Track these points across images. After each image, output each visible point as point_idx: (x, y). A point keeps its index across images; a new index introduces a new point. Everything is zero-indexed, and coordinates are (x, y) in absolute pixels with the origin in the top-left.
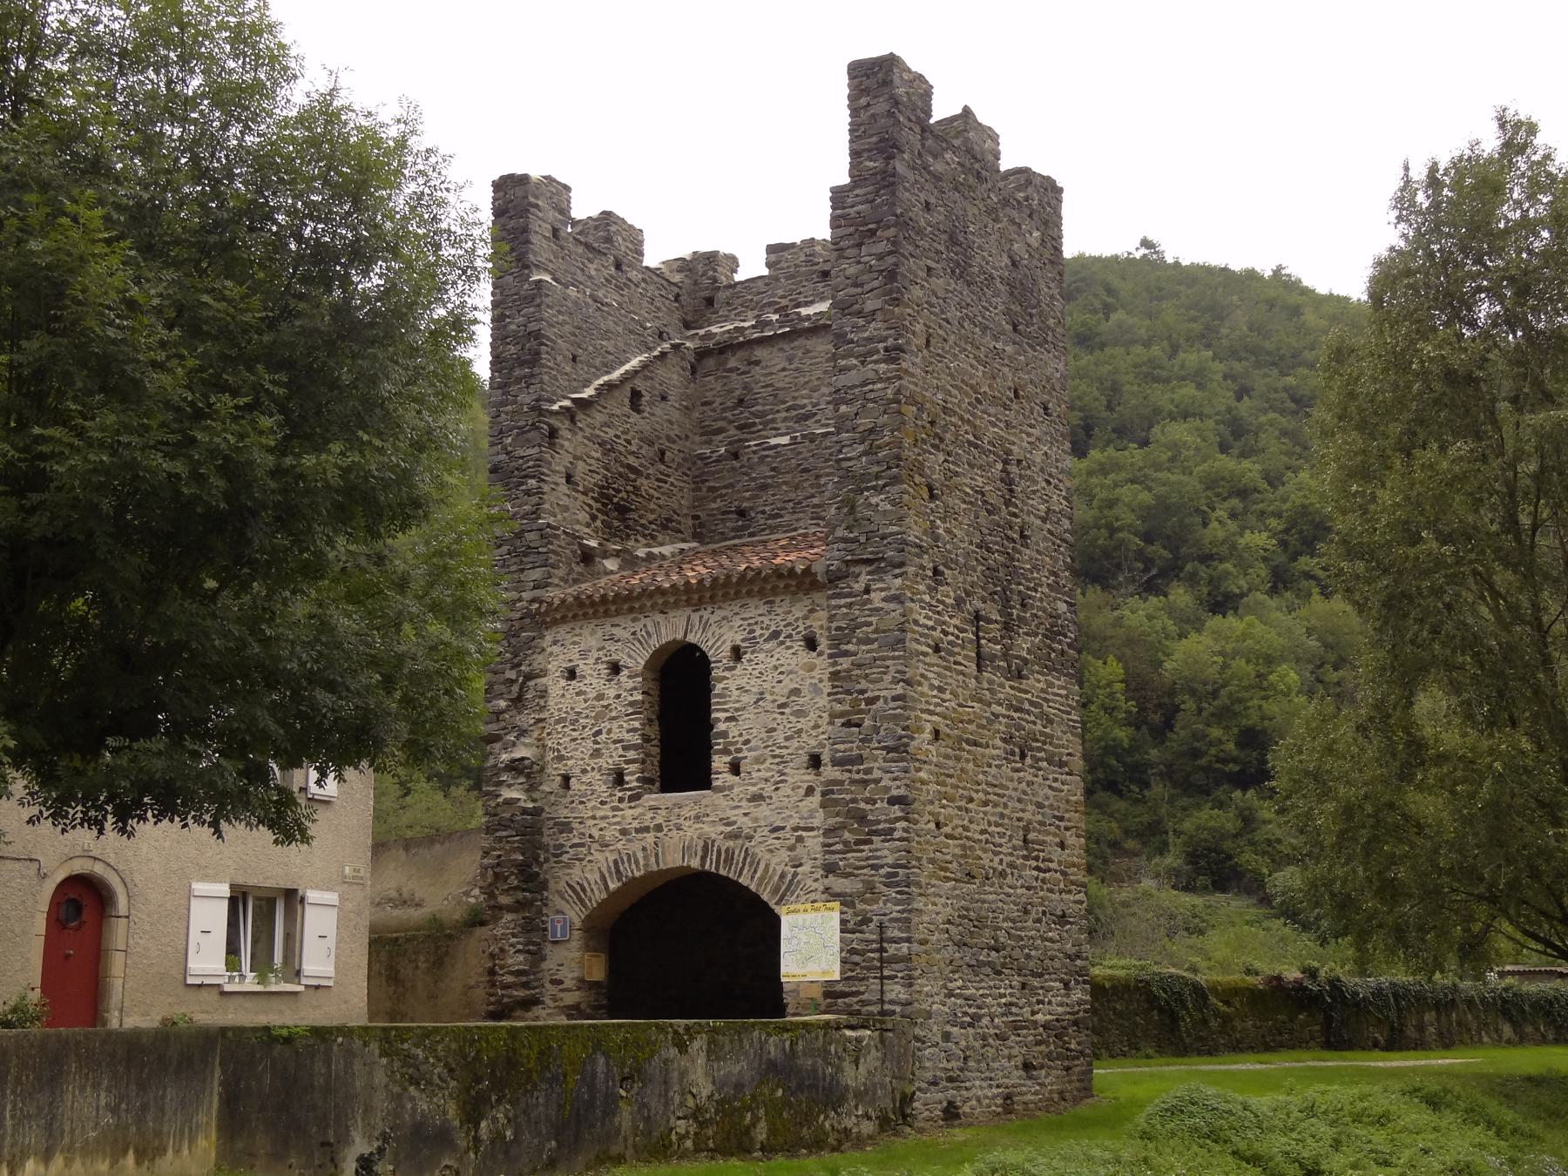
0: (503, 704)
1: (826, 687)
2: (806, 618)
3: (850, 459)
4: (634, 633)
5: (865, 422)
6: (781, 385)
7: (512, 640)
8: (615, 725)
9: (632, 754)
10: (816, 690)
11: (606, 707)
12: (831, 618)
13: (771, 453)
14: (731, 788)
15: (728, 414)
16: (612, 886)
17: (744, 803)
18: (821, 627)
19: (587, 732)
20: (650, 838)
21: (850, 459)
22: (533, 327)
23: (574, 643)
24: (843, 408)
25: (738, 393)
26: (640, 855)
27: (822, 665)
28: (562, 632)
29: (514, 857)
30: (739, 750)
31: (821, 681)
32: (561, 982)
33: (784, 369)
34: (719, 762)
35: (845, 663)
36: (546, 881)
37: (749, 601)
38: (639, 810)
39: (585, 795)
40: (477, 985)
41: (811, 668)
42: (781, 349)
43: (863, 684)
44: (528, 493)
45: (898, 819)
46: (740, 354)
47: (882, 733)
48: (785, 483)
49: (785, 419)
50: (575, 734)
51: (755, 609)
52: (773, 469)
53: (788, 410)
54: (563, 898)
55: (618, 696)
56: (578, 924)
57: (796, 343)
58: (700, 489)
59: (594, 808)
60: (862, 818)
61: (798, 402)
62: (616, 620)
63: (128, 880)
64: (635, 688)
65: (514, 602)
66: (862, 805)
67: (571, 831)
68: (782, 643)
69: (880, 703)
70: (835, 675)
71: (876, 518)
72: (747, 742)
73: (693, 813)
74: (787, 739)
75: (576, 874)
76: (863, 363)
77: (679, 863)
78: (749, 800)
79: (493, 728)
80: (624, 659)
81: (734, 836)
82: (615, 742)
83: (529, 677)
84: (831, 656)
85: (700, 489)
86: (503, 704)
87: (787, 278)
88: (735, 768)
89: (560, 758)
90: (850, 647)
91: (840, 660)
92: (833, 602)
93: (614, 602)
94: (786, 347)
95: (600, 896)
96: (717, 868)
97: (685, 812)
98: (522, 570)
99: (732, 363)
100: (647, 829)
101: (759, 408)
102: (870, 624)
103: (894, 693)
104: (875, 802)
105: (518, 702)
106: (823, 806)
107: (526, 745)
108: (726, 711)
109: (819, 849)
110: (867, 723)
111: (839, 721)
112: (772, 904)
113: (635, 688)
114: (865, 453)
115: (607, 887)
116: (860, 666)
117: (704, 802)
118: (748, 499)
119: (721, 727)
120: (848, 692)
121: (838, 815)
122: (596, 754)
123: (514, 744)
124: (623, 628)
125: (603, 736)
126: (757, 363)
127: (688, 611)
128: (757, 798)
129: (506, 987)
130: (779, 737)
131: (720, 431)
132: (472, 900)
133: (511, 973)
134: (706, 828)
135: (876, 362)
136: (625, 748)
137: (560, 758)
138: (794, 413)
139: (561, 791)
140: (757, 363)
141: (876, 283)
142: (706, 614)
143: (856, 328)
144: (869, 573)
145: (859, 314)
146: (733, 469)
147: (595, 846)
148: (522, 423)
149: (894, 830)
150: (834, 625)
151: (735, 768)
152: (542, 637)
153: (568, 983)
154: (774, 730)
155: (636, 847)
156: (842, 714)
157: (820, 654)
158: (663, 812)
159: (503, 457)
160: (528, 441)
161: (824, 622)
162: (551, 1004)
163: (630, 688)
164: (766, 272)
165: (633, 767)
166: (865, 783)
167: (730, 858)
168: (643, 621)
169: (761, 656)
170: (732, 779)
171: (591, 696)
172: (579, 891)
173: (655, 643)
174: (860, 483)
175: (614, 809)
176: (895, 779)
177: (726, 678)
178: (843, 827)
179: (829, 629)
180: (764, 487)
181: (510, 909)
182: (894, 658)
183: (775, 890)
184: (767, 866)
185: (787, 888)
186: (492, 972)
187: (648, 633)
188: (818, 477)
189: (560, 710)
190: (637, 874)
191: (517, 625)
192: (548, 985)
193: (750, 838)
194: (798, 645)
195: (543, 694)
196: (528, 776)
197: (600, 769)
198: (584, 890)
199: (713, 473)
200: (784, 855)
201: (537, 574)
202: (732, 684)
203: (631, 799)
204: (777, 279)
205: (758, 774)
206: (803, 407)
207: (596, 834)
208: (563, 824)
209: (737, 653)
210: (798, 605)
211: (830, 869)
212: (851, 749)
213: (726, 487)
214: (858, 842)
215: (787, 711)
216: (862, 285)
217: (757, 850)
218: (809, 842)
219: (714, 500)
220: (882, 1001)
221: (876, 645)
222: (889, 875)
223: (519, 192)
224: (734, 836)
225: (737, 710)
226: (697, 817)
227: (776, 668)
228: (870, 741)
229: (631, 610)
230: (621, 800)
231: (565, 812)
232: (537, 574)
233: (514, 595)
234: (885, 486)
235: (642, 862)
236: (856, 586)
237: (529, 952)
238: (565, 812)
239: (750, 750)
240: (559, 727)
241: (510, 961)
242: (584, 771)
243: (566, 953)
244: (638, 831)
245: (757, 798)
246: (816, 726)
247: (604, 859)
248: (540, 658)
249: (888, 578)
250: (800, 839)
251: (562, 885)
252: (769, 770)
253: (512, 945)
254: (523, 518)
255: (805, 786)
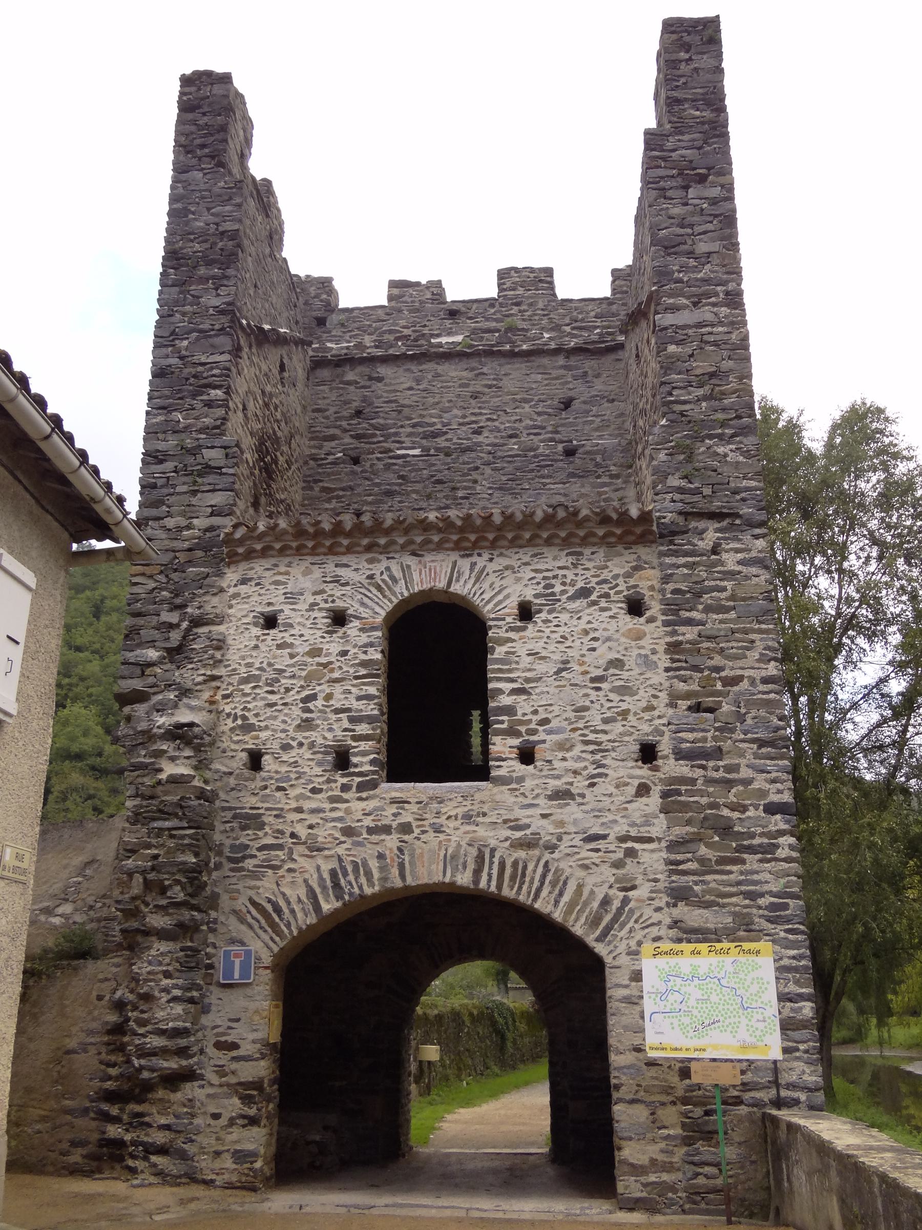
0: (153, 654)
1: (663, 661)
2: (628, 575)
3: (685, 402)
4: (371, 577)
5: (701, 366)
6: (406, 402)
7: (175, 576)
8: (338, 689)
9: (363, 729)
10: (647, 663)
11: (325, 665)
12: (666, 579)
13: (399, 461)
14: (521, 780)
15: (344, 424)
16: (326, 907)
17: (541, 801)
18: (652, 588)
19: (291, 697)
20: (391, 841)
21: (685, 402)
22: (228, 226)
23: (277, 583)
24: (672, 348)
25: (355, 404)
26: (374, 864)
27: (654, 633)
28: (258, 568)
29: (182, 858)
30: (534, 732)
31: (654, 652)
32: (234, 1046)
33: (410, 389)
34: (501, 746)
35: (689, 634)
36: (215, 897)
37: (545, 550)
38: (371, 805)
39: (288, 779)
40: (84, 1047)
41: (639, 636)
42: (408, 370)
43: (717, 660)
44: (209, 404)
45: (782, 833)
46: (360, 369)
47: (749, 721)
48: (414, 491)
49: (410, 435)
50: (273, 698)
51: (554, 561)
52: (402, 477)
53: (414, 426)
54: (242, 921)
55: (344, 653)
56: (267, 959)
57: (424, 367)
58: (311, 489)
59: (298, 798)
60: (726, 829)
61: (427, 420)
62: (344, 559)
63: (400, 348)
64: (371, 645)
65: (180, 529)
66: (726, 812)
67: (261, 826)
68: (594, 603)
69: (745, 684)
70: (674, 648)
71: (726, 470)
72: (545, 722)
73: (460, 811)
74: (606, 721)
75: (266, 887)
76: (695, 304)
77: (437, 878)
78: (550, 798)
79: (137, 684)
80: (352, 606)
81: (528, 844)
82: (337, 711)
83: (197, 622)
84: (666, 624)
85: (311, 489)
86: (153, 654)
87: (410, 311)
88: (527, 756)
89: (247, 728)
90: (694, 615)
91: (682, 629)
92: (668, 560)
93: (348, 535)
94: (414, 368)
95: (305, 919)
96: (499, 886)
97: (448, 809)
98: (194, 493)
99: (350, 376)
100: (387, 830)
101: (381, 421)
102: (724, 589)
103: (764, 673)
104: (744, 809)
105: (176, 654)
106: (665, 810)
107: (191, 708)
108: (512, 680)
109: (662, 867)
110: (726, 708)
111: (683, 704)
112: (590, 940)
113: (371, 645)
114: (705, 398)
115: (317, 907)
116: (709, 638)
117: (478, 796)
118: (370, 503)
119: (506, 700)
120: (696, 668)
121: (689, 822)
122: (306, 725)
123: (176, 706)
124: (356, 570)
125: (319, 703)
126: (380, 379)
127: (454, 556)
128: (562, 795)
129: (144, 1053)
130: (595, 717)
131: (333, 438)
132: (56, 921)
133: (162, 1033)
134: (481, 832)
135: (714, 305)
136: (352, 720)
137: (247, 728)
138: (421, 430)
139: (247, 773)
140: (380, 379)
141: (710, 227)
142: (481, 562)
143: (683, 268)
144: (717, 530)
145: (690, 254)
146: (354, 473)
147: (301, 849)
148: (206, 326)
149: (777, 846)
150: (670, 587)
151: (527, 756)
152: (220, 574)
153: (246, 1049)
154: (585, 709)
155: (368, 853)
156: (687, 696)
157: (651, 620)
158: (414, 808)
159: (174, 361)
160: (213, 346)
161: (656, 583)
162: (215, 1080)
163: (364, 643)
164: (385, 302)
165: (364, 746)
166: (729, 784)
167: (519, 873)
168: (385, 563)
169: (564, 617)
170: (521, 769)
171: (300, 650)
172: (269, 915)
173: (402, 591)
174: (700, 430)
175: (332, 799)
176: (774, 781)
177: (513, 641)
178: (697, 839)
179: (662, 591)
180: (389, 494)
181: (163, 935)
182: (760, 631)
183: (594, 922)
184: (580, 887)
185: (612, 915)
186: (119, 1029)
187: (393, 578)
188: (454, 489)
189: (249, 665)
190: (368, 891)
191: (183, 558)
192: (211, 1050)
193: (552, 848)
194: (618, 608)
195: (220, 644)
196: (197, 749)
197: (312, 745)
198: (278, 911)
199: (329, 474)
200: (608, 873)
201: (218, 499)
202: (522, 649)
203: (361, 787)
204: (400, 311)
205: (561, 765)
206: (434, 424)
207: (302, 832)
208: (248, 817)
209: (526, 613)
210: (616, 560)
211: (679, 895)
212: (705, 740)
213: (343, 489)
214: (722, 861)
215: (605, 686)
216: (691, 226)
217: (562, 865)
218: (645, 857)
219: (329, 500)
220: (776, 1083)
221: (733, 615)
222: (773, 907)
223: (218, 90)
224: (528, 844)
225: (528, 680)
226: (468, 818)
227: (586, 632)
228: (732, 731)
229: (369, 548)
230: (345, 788)
231: (253, 801)
232: (218, 499)
233: (183, 522)
234: (733, 436)
235: (376, 875)
236: (701, 544)
237: (191, 1001)
238: (253, 801)
239: (550, 732)
240: (247, 688)
241: (160, 1014)
242: (286, 747)
243: (243, 1003)
244: (371, 831)
245: (562, 795)
246: (650, 708)
247: (312, 868)
248: (215, 601)
249: (746, 537)
250: (631, 853)
251: (241, 903)
252: (579, 759)
253: (166, 990)
254: (200, 431)
255: (636, 782)
